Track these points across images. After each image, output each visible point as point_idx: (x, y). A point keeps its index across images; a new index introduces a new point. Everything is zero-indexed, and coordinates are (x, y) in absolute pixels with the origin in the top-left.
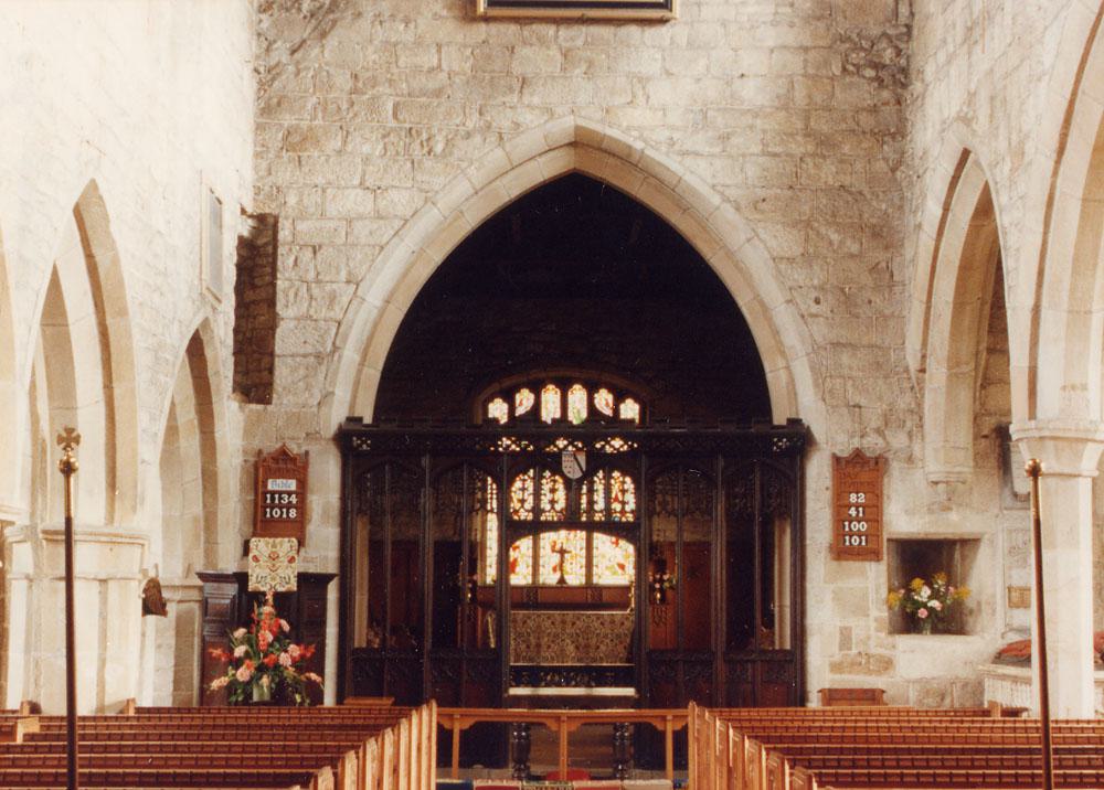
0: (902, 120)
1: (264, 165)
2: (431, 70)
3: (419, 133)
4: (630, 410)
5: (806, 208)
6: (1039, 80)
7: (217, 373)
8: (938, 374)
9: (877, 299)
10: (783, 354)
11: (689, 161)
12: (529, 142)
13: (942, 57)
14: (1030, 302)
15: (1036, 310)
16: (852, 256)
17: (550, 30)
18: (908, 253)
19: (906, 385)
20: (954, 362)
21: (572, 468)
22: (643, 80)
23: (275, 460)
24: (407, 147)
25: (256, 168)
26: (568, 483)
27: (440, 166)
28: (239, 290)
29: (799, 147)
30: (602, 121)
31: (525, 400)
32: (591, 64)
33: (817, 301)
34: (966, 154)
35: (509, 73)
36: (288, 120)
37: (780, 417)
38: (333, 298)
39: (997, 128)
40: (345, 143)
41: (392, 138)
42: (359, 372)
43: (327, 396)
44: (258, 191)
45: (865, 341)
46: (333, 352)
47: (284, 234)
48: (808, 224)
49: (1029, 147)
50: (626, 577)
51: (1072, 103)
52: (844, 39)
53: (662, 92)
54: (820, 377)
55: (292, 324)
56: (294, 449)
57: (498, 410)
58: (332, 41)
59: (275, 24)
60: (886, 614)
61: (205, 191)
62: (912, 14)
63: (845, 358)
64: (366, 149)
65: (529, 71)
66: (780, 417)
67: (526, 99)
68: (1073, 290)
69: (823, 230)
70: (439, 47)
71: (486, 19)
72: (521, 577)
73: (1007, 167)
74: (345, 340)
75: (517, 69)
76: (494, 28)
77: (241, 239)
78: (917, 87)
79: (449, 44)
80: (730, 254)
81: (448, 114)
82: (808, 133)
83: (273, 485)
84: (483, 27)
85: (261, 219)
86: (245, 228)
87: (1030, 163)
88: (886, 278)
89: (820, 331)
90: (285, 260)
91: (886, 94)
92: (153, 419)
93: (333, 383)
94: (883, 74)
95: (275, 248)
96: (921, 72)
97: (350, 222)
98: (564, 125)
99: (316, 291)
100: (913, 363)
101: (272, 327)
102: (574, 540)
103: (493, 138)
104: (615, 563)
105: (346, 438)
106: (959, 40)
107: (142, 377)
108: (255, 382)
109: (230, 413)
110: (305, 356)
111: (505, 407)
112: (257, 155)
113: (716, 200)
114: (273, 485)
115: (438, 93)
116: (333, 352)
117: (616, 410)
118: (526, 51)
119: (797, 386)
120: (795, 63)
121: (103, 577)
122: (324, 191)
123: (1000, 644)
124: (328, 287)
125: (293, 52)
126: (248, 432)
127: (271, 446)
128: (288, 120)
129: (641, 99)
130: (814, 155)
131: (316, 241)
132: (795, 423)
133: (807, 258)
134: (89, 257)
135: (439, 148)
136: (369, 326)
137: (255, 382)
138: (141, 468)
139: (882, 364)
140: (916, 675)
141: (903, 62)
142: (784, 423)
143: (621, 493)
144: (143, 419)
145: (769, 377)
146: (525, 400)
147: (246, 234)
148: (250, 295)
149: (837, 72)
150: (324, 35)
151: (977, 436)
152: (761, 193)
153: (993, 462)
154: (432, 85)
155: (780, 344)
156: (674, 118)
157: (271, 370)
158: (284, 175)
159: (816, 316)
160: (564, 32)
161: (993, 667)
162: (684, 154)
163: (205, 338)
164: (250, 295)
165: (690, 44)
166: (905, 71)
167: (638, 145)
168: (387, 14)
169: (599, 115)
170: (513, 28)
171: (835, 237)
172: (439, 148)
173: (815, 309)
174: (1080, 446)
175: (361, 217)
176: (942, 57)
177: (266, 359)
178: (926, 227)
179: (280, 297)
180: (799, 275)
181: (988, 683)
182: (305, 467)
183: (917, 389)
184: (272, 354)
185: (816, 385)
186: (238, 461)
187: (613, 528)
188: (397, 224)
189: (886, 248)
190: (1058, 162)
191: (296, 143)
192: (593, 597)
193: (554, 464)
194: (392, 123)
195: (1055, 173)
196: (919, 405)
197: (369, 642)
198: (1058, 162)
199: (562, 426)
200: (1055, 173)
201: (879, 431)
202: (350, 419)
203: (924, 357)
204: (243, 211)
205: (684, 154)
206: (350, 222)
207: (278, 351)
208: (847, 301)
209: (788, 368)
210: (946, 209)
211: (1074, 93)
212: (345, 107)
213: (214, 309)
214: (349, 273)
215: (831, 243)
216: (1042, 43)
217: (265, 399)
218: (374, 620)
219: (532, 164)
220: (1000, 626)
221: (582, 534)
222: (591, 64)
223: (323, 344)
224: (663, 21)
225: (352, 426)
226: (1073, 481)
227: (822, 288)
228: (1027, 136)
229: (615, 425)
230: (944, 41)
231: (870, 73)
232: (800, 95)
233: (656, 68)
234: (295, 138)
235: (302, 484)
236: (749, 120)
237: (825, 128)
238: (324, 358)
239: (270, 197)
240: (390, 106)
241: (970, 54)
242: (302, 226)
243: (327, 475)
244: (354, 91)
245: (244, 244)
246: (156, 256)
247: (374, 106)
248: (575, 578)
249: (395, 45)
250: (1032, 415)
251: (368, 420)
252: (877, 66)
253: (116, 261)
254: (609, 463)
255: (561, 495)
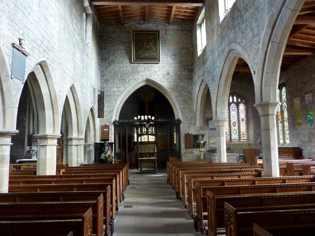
0: (192, 76)
1: (102, 84)
2: (126, 70)
3: (124, 79)
4: (153, 118)
5: (179, 89)
6: (217, 67)
7: (95, 114)
8: (198, 112)
9: (190, 102)
10: (176, 109)
11: (163, 83)
12: (140, 80)
13: (199, 67)
14: (215, 100)
15: (217, 101)
16: (186, 96)
17: (142, 65)
18: (194, 95)
19: (194, 114)
20: (201, 110)
21: (147, 126)
22: (156, 72)
23: (105, 126)
24: (122, 81)
25: (100, 85)
26: (146, 128)
27: (127, 84)
28: (98, 102)
29: (178, 81)
30: (150, 77)
31: (139, 117)
32: (148, 69)
33: (181, 102)
34: (203, 80)
35: (137, 71)
36: (105, 78)
37: (176, 118)
38: (112, 103)
39: (209, 76)
40: (113, 81)
41: (120, 80)
42: (116, 113)
43: (112, 117)
44: (101, 88)
45: (188, 107)
46: (112, 111)
47: (105, 94)
48: (180, 91)
49: (215, 78)
50: (154, 140)
51: (222, 70)
52: (183, 65)
53: (158, 73)
54: (182, 113)
55: (106, 107)
56: (107, 125)
57: (136, 118)
58: (111, 67)
59: (103, 64)
60: (217, 162)
61: (92, 87)
62: (193, 62)
63: (185, 110)
64: (116, 82)
65: (139, 70)
66: (176, 118)
67: (139, 74)
68: (222, 98)
69: (182, 92)
70: (127, 67)
71: (133, 63)
72: (139, 140)
73: (211, 81)
74: (114, 109)
75: (138, 70)
76: (134, 64)
77: (98, 95)
78: (195, 72)
79: (128, 67)
80: (169, 96)
81: (128, 77)
82: (179, 79)
83: (104, 130)
84: (133, 64)
85: (101, 92)
86: (99, 93)
87: (215, 80)
88: (191, 99)
89: (182, 106)
90: (105, 98)
91: (190, 73)
92: (84, 121)
93: (113, 115)
94: (190, 70)
95: (104, 96)
96: (195, 70)
97: (114, 92)
98: (145, 78)
99: (110, 102)
100: (195, 110)
101: (103, 107)
102: (146, 136)
103: (135, 80)
104: (152, 139)
105: (114, 123)
106: (201, 64)
107: (82, 114)
108: (101, 115)
109: (98, 120)
110: (108, 111)
111: (136, 118)
112: (101, 83)
113: (167, 88)
114: (104, 130)
115: (127, 74)
116: (112, 111)
117: (151, 118)
118: (139, 68)
119: (179, 114)
120: (177, 69)
121: (77, 144)
122: (111, 88)
123: (208, 149)
124: (112, 101)
125: (106, 68)
126: (100, 122)
127: (104, 124)
128: (105, 78)
129: (155, 74)
130: (180, 82)
131: (110, 95)
132: (179, 119)
133: (180, 96)
134: (73, 96)
135: (127, 81)
136: (118, 107)
137: (101, 115)
138: (83, 128)
139: (191, 110)
140: (196, 154)
141: (192, 68)
142: (177, 119)
143: (152, 130)
144: (83, 121)
145: (175, 113)
146: (139, 117)
147: (99, 94)
148: (100, 103)
149: (183, 70)
150: (110, 66)
151: (204, 120)
152: (173, 87)
153: (206, 124)
154: (126, 73)
155: (176, 108)
156: (160, 77)
157: (103, 113)
158: (105, 86)
159: (181, 104)
160: (144, 65)
161: (207, 153)
162: (162, 82)
163: (93, 109)
164: (100, 103)
165: (162, 66)
166: (192, 70)
167: (155, 81)
168: (119, 62)
169: (150, 76)
170: (137, 64)
171: (183, 93)
172: (127, 81)
173: (181, 103)
174: (224, 122)
175: (116, 91)
176: (199, 67)
177: (103, 112)
178: (197, 91)
179: (105, 103)
180: (179, 98)
181: (206, 155)
182: (109, 127)
183: (195, 114)
184: (104, 111)
185: (181, 114)
186: (99, 126)
187: (152, 135)
188: (121, 92)
189: (191, 94)
190: (220, 80)
191: (106, 81)
192: (149, 143)
193: (144, 126)
194: (120, 78)
195: (219, 81)
196: (196, 116)
197: (119, 152)
198: (220, 80)
199: (145, 120)
200: (219, 81)
201: (190, 120)
202: (115, 120)
203: (196, 109)
204: (99, 91)
205: (162, 82)
206: (114, 92)
207: (104, 111)
208: (185, 102)
209: (177, 111)
210: (200, 88)
211: (223, 69)
212: (113, 76)
213: (94, 104)
214: (115, 99)
215: (183, 94)
216: (217, 62)
217: (103, 117)
218: (119, 148)
219: (140, 84)
220: (208, 147)
221: (147, 136)
222: (148, 69)
223: (111, 110)
224: (158, 63)
225: (116, 121)
226: (223, 127)
227: (182, 100)
228: (214, 76)
229: (151, 120)
230: (199, 65)
231: (188, 70)
232: (178, 73)
233: (158, 70)
234: (106, 80)
235: (109, 129)
236: (171, 77)
237: (181, 78)
238: (111, 112)
239: (103, 89)
240: (120, 76)
241: (203, 66)
242: (108, 93)
243: (112, 128)
244: (115, 73)
245: (99, 95)
246: (84, 96)
247: (118, 76)
248: (146, 140)
249: (120, 67)
250: (216, 117)
251: (118, 120)
252: (189, 69)
253: (78, 97)
254: (151, 125)
255: (145, 130)
